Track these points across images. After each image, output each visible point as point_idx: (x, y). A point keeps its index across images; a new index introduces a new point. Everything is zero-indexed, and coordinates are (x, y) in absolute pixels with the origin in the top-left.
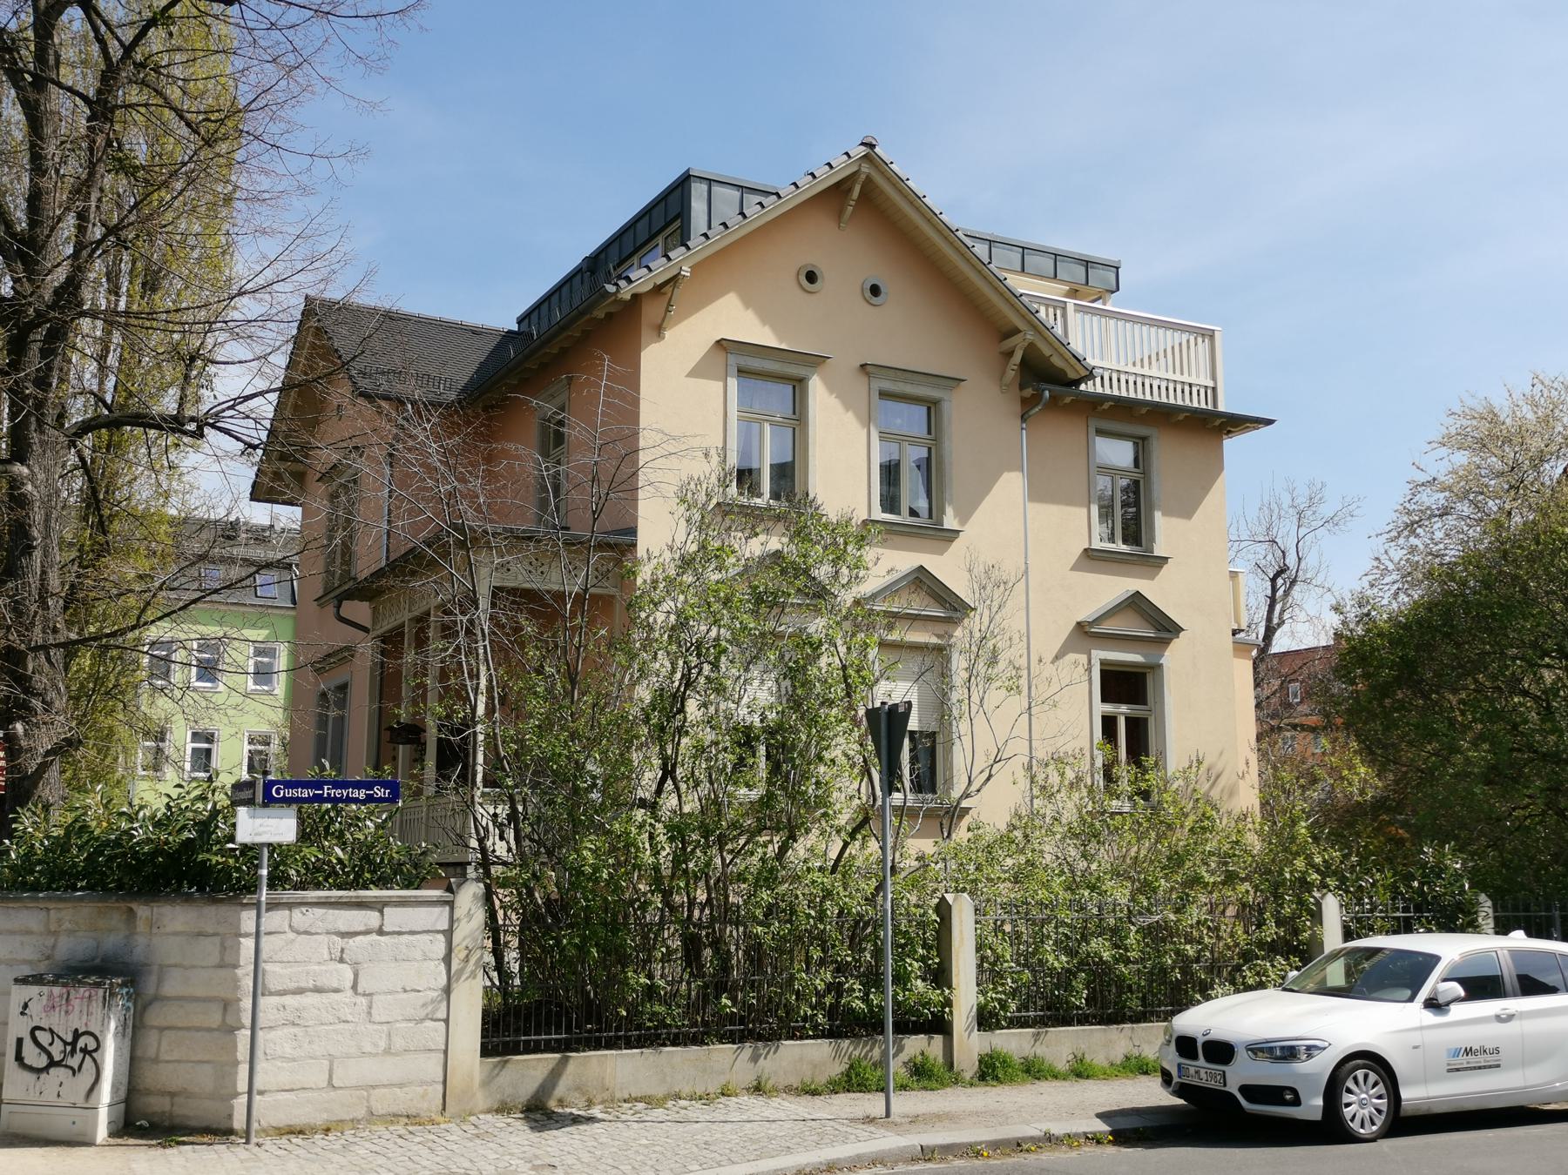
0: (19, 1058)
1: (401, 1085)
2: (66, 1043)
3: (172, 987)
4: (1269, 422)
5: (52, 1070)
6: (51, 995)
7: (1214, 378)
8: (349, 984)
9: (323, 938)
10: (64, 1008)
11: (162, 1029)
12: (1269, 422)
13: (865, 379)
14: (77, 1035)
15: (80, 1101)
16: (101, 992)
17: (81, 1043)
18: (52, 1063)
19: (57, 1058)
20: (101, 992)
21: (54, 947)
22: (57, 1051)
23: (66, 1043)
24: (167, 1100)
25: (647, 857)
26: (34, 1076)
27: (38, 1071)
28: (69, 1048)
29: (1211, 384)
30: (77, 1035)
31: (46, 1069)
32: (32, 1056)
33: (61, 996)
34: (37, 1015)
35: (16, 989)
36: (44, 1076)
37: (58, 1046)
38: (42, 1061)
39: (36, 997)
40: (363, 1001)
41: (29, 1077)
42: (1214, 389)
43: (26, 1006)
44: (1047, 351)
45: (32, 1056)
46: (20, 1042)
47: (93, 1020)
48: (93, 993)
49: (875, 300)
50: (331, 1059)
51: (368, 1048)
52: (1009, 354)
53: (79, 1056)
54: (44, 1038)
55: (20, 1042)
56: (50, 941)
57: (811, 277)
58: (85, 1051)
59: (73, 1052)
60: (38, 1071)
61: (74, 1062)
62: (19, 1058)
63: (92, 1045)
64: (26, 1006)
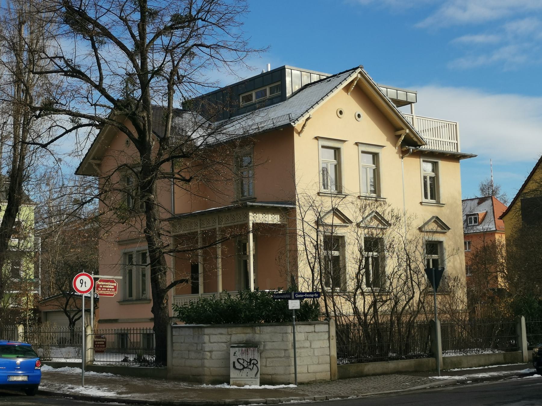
0: (234, 367)
1: (321, 372)
2: (248, 362)
3: (269, 346)
4: (476, 156)
5: (244, 369)
6: (242, 350)
7: (457, 140)
8: (309, 346)
9: (303, 334)
10: (246, 353)
11: (266, 358)
12: (476, 156)
13: (357, 147)
14: (251, 360)
15: (254, 376)
16: (257, 349)
17: (252, 362)
18: (244, 368)
19: (246, 366)
20: (257, 349)
21: (230, 338)
22: (245, 364)
23: (248, 362)
24: (270, 376)
25: (324, 310)
26: (239, 371)
27: (240, 370)
28: (249, 364)
29: (456, 142)
30: (251, 360)
31: (243, 369)
32: (238, 366)
33: (245, 350)
34: (239, 355)
35: (231, 349)
36: (242, 371)
37: (245, 363)
38: (242, 367)
39: (238, 351)
40: (312, 350)
41: (238, 372)
42: (457, 144)
43: (235, 353)
44: (412, 136)
45: (238, 366)
46: (234, 363)
47: (255, 356)
48: (255, 349)
49: (359, 119)
50: (308, 365)
51: (315, 363)
52: (400, 136)
53: (252, 365)
54: (241, 361)
55: (234, 363)
56: (229, 337)
57: (341, 113)
58: (254, 364)
59: (250, 364)
60: (240, 370)
61: (251, 367)
62: (234, 367)
63: (255, 362)
64: (235, 353)
